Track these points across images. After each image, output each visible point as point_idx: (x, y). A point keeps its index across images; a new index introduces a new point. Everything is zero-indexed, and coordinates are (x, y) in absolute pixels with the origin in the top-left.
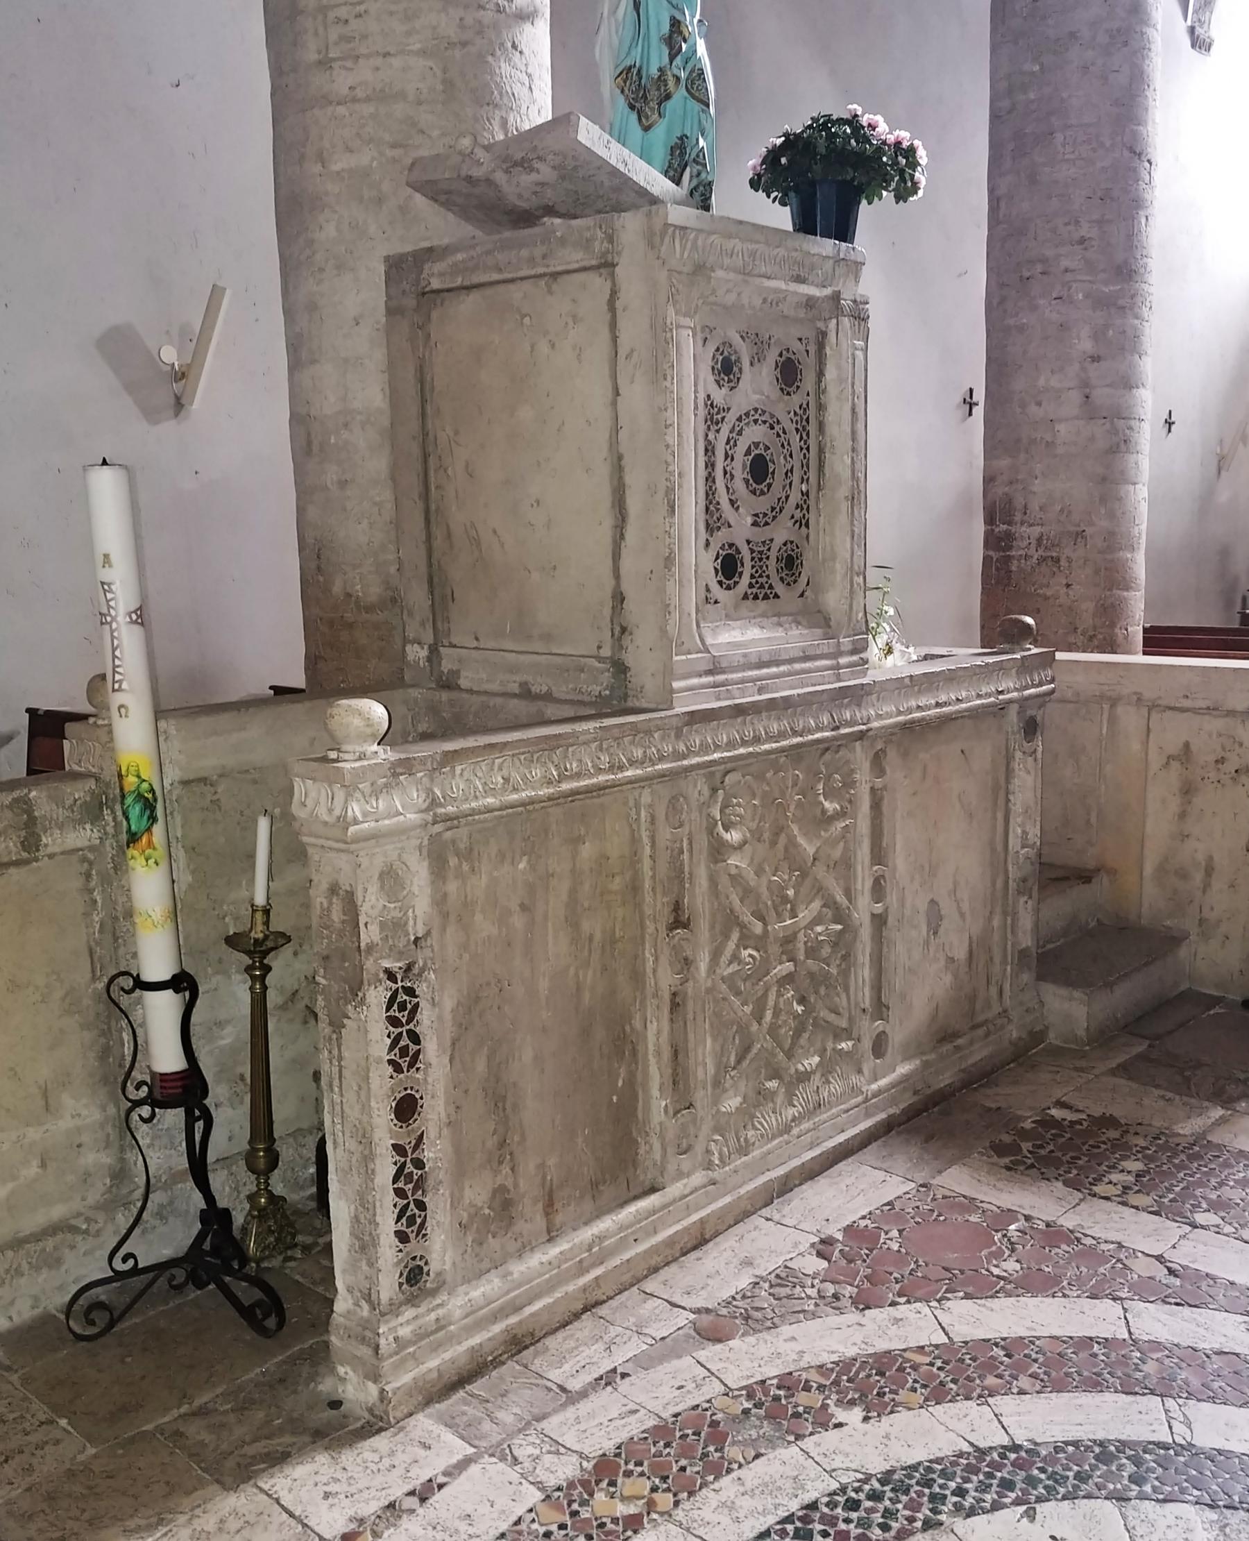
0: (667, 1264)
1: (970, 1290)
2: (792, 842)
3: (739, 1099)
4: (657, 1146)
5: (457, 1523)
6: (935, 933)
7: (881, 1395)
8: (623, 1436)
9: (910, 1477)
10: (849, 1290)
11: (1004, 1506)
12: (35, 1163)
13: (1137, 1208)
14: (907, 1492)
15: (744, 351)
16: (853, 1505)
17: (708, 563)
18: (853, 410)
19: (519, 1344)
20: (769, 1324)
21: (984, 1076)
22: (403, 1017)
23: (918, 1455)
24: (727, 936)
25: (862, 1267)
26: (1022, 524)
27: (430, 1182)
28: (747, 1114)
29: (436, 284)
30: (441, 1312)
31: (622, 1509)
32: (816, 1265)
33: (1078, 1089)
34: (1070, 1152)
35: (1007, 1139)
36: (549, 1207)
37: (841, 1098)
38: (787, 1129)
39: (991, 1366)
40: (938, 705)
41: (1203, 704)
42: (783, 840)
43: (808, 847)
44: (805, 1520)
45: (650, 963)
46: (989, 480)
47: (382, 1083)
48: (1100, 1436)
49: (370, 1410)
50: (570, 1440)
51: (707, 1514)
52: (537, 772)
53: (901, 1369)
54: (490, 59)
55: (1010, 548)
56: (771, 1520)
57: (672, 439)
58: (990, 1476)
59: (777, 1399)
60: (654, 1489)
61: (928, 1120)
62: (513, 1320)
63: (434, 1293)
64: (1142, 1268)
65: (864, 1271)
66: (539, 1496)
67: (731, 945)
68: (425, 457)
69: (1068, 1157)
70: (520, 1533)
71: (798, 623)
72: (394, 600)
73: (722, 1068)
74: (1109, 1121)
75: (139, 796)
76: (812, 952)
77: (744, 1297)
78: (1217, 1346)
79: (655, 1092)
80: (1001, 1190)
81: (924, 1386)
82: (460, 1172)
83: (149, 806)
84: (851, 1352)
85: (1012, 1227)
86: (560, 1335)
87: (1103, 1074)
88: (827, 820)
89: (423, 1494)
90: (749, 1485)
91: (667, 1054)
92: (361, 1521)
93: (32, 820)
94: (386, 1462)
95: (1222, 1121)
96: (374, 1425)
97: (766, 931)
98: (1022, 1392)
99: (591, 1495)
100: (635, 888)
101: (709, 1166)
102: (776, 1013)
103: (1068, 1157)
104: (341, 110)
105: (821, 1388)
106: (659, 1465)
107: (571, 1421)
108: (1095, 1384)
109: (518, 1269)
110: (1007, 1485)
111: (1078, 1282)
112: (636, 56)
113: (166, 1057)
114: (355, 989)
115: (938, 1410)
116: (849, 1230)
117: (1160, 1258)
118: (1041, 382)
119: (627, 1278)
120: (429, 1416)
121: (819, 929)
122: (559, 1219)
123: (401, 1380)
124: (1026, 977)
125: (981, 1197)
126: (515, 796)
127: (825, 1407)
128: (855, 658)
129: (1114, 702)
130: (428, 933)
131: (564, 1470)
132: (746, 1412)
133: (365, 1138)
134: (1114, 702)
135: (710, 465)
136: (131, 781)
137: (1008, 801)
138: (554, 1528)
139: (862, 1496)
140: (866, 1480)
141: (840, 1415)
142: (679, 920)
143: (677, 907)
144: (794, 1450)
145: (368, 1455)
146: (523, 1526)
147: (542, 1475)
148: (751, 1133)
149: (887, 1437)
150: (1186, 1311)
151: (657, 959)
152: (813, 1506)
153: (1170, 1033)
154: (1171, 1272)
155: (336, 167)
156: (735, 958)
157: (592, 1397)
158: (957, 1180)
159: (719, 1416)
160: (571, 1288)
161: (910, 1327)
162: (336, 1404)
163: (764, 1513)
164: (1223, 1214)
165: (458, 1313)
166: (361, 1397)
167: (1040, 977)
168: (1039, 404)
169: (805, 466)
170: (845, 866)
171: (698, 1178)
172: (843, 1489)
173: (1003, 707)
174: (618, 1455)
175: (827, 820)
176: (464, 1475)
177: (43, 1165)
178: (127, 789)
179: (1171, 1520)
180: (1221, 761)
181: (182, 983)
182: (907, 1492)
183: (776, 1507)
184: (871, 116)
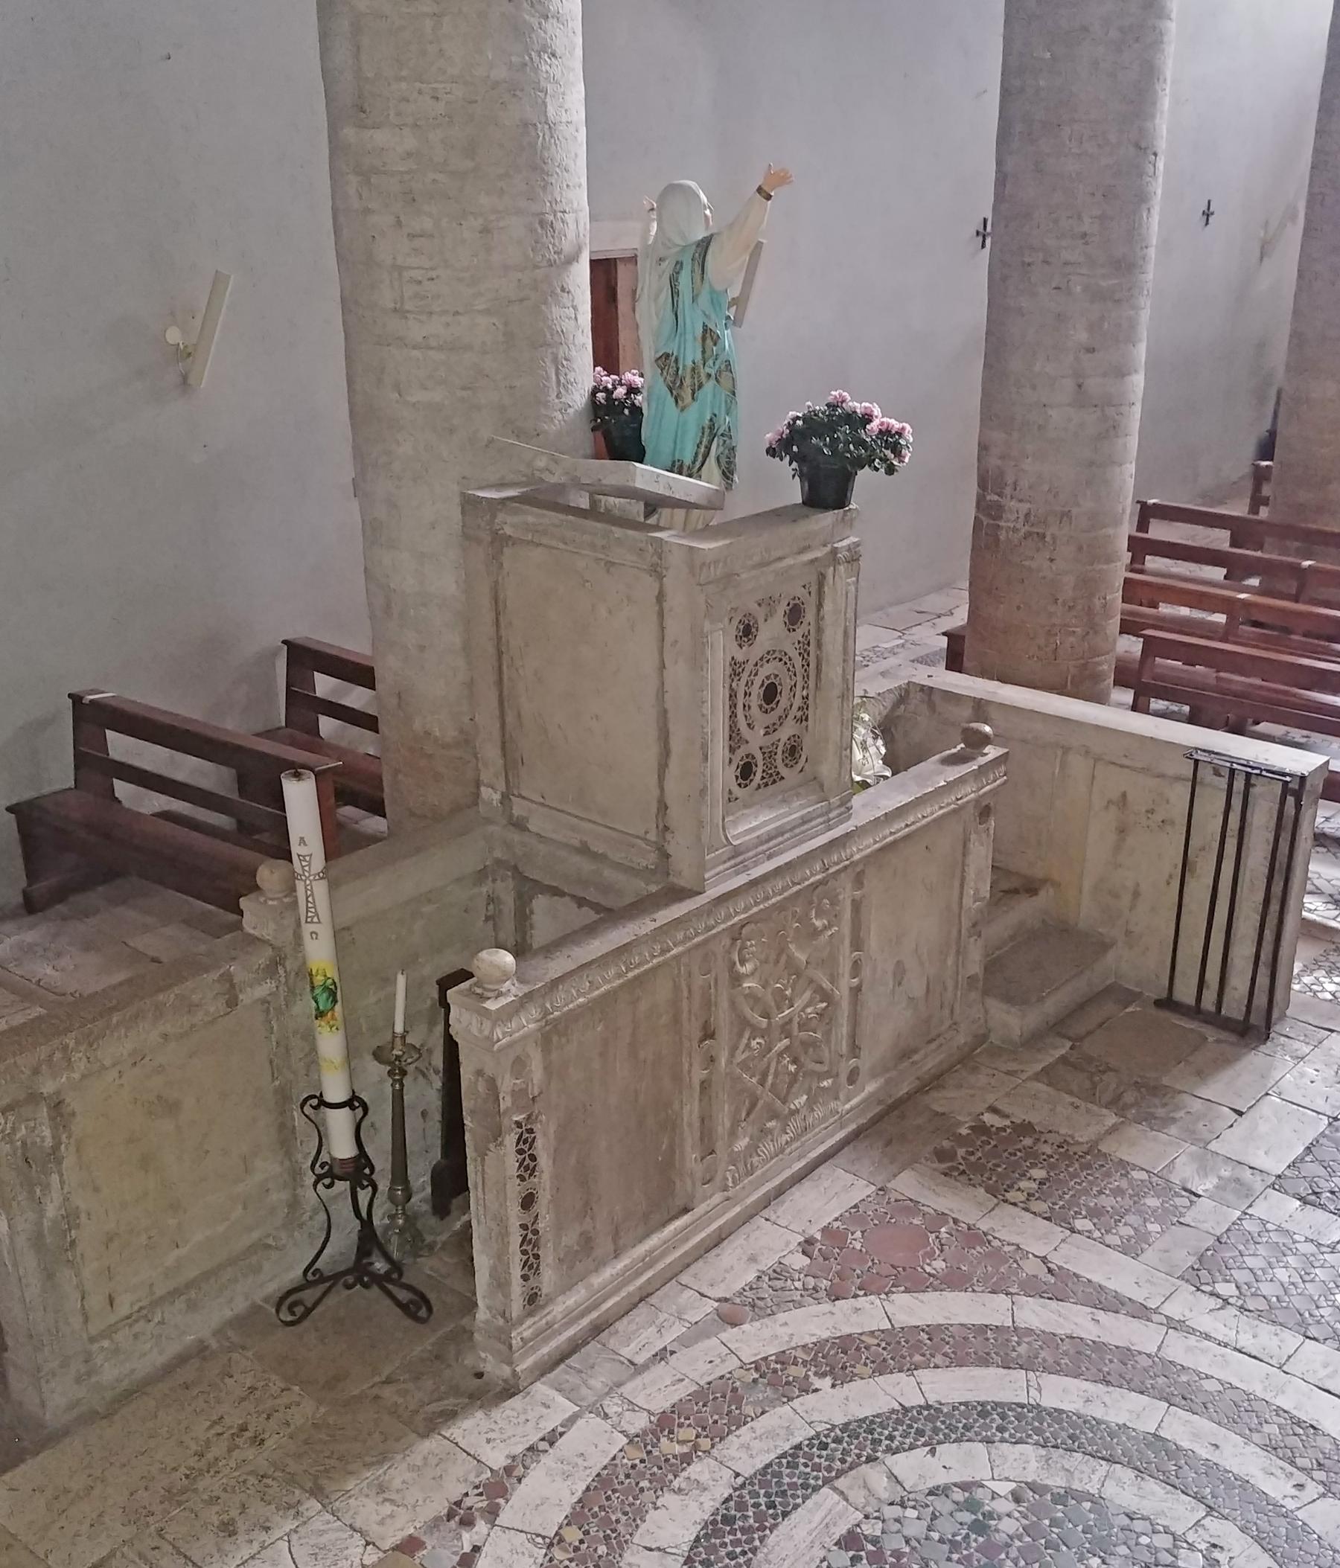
0: (697, 1260)
1: (908, 1285)
2: (790, 959)
3: (747, 1139)
4: (689, 1182)
5: (576, 1459)
6: (900, 984)
7: (844, 1368)
8: (675, 1399)
9: (860, 1427)
10: (824, 1284)
11: (918, 1447)
12: (240, 1207)
13: (1034, 1213)
14: (857, 1438)
15: (760, 613)
16: (824, 1446)
17: (732, 772)
18: (846, 633)
19: (597, 1330)
20: (769, 1311)
21: (934, 1081)
22: (526, 1147)
23: (866, 1412)
24: (740, 1035)
25: (837, 1263)
26: (1012, 498)
27: (542, 1241)
28: (753, 1149)
29: (508, 530)
30: (549, 1318)
31: (678, 1449)
32: (800, 1261)
33: (1008, 1095)
34: (996, 1160)
35: (946, 1144)
36: (616, 1236)
37: (824, 1119)
38: (782, 1151)
39: (917, 1347)
40: (907, 826)
41: (1139, 765)
42: (784, 958)
43: (801, 957)
44: (794, 1456)
45: (686, 1066)
46: (983, 447)
47: (514, 1191)
48: (982, 1399)
49: (505, 1381)
50: (640, 1401)
51: (733, 1452)
52: (612, 972)
53: (858, 1349)
54: (543, 307)
55: (1000, 518)
56: (773, 1456)
57: (707, 710)
58: (910, 1426)
59: (775, 1371)
60: (697, 1436)
61: (891, 1128)
62: (594, 1315)
63: (543, 1307)
64: (1032, 1267)
65: (836, 1268)
66: (625, 1440)
67: (745, 1041)
68: (500, 654)
69: (990, 1165)
70: (616, 1465)
71: (798, 795)
72: (467, 740)
73: (736, 1123)
74: (1025, 1128)
75: (326, 988)
76: (802, 1027)
77: (751, 1289)
78: (1069, 1332)
79: (688, 1149)
80: (938, 1195)
81: (873, 1362)
82: (559, 1228)
83: (332, 994)
84: (825, 1335)
85: (943, 1230)
86: (625, 1320)
87: (1029, 1079)
88: (816, 933)
89: (552, 1439)
90: (758, 1433)
91: (697, 1124)
92: (514, 1458)
93: (233, 986)
94: (522, 1418)
95: (1113, 1130)
96: (509, 1391)
97: (769, 1024)
98: (936, 1367)
99: (658, 1440)
100: (676, 1020)
101: (725, 1189)
102: (776, 1075)
103: (990, 1165)
104: (416, 353)
105: (805, 1363)
106: (701, 1418)
107: (641, 1387)
108: (984, 1362)
109: (597, 1280)
110: (920, 1433)
111: (985, 1279)
112: (672, 348)
113: (342, 1148)
114: (497, 1135)
115: (880, 1379)
116: (825, 1230)
117: (1044, 1260)
118: (1037, 368)
119: (668, 1275)
120: (543, 1383)
121: (809, 1010)
122: (621, 1242)
123: (524, 1365)
124: (974, 995)
125: (922, 1201)
126: (597, 993)
127: (807, 1377)
128: (843, 809)
129: (1066, 750)
130: (541, 1093)
131: (639, 1423)
132: (755, 1381)
133: (502, 1222)
134: (1066, 750)
135: (733, 706)
136: (319, 980)
137: (963, 871)
138: (637, 1462)
139: (829, 1440)
140: (831, 1430)
141: (817, 1383)
142: (708, 1034)
143: (706, 1025)
144: (787, 1407)
145: (508, 1412)
146: (617, 1461)
147: (625, 1426)
148: (755, 1159)
149: (847, 1399)
150: (1054, 1304)
151: (691, 1065)
152: (798, 1447)
153: (1089, 1033)
154: (1050, 1271)
155: (413, 399)
156: (748, 1045)
157: (653, 1369)
158: (906, 1184)
159: (738, 1384)
160: (631, 1288)
161: (866, 1315)
162: (480, 1375)
163: (768, 1451)
164: (1095, 1220)
165: (560, 1316)
166: (498, 1372)
167: (986, 993)
168: (1034, 387)
169: (806, 677)
170: (829, 964)
171: (718, 1198)
172: (818, 1435)
173: (962, 808)
174: (673, 1412)
175: (816, 933)
176: (575, 1427)
177: (245, 1208)
178: (316, 984)
179: (1017, 1456)
180: (1152, 811)
181: (353, 1102)
182: (857, 1438)
183: (776, 1447)
184: (867, 404)
